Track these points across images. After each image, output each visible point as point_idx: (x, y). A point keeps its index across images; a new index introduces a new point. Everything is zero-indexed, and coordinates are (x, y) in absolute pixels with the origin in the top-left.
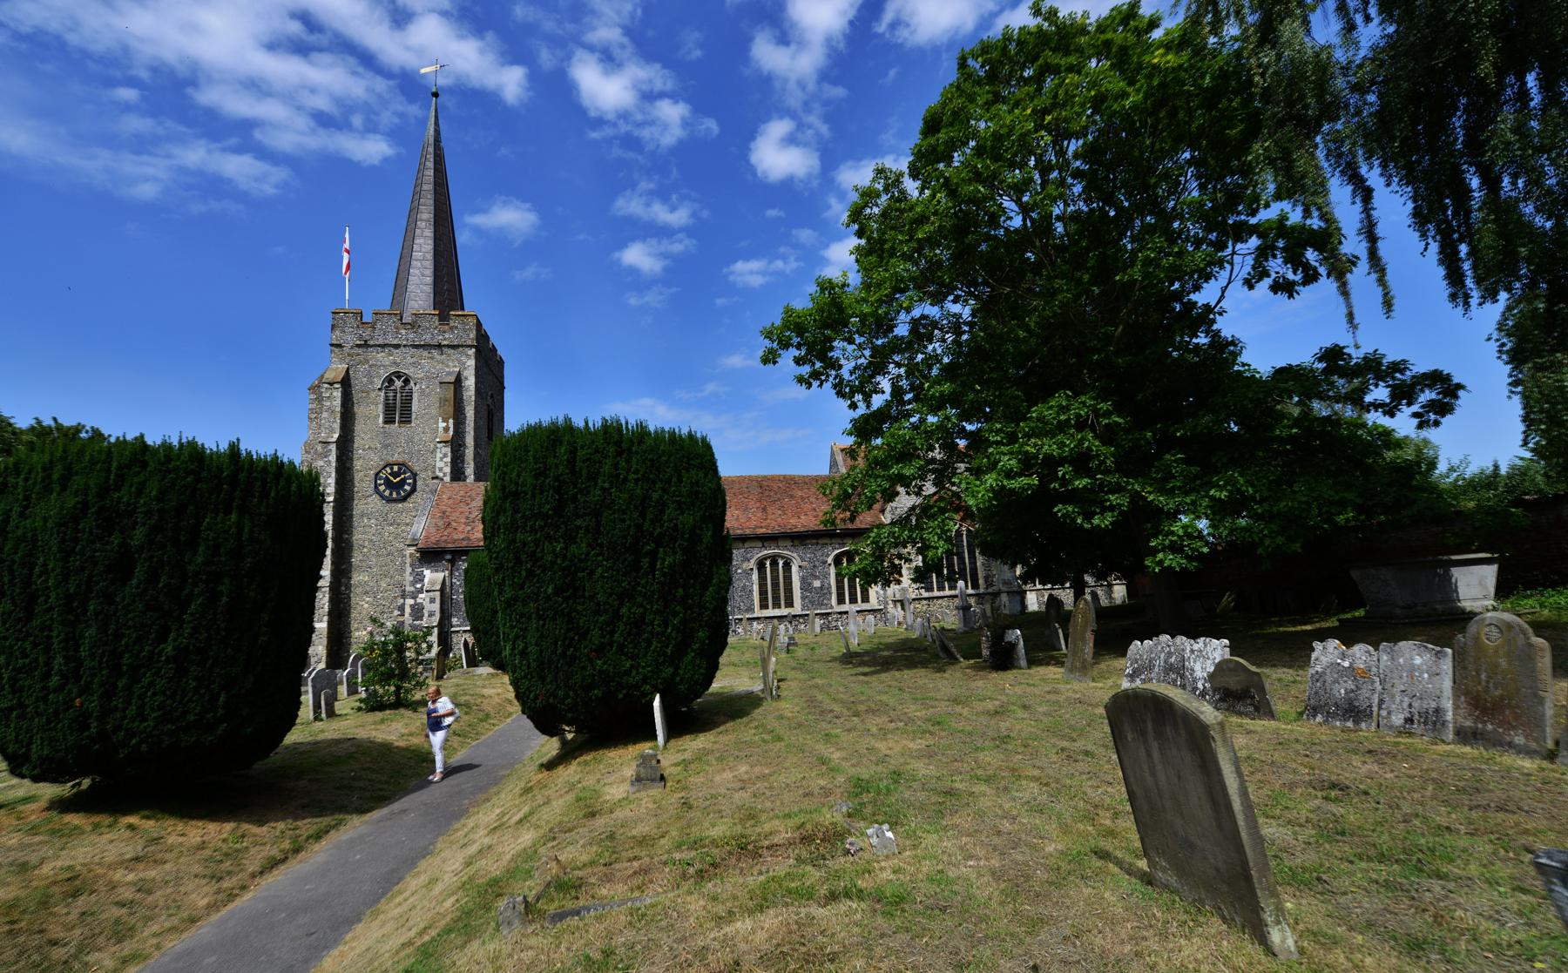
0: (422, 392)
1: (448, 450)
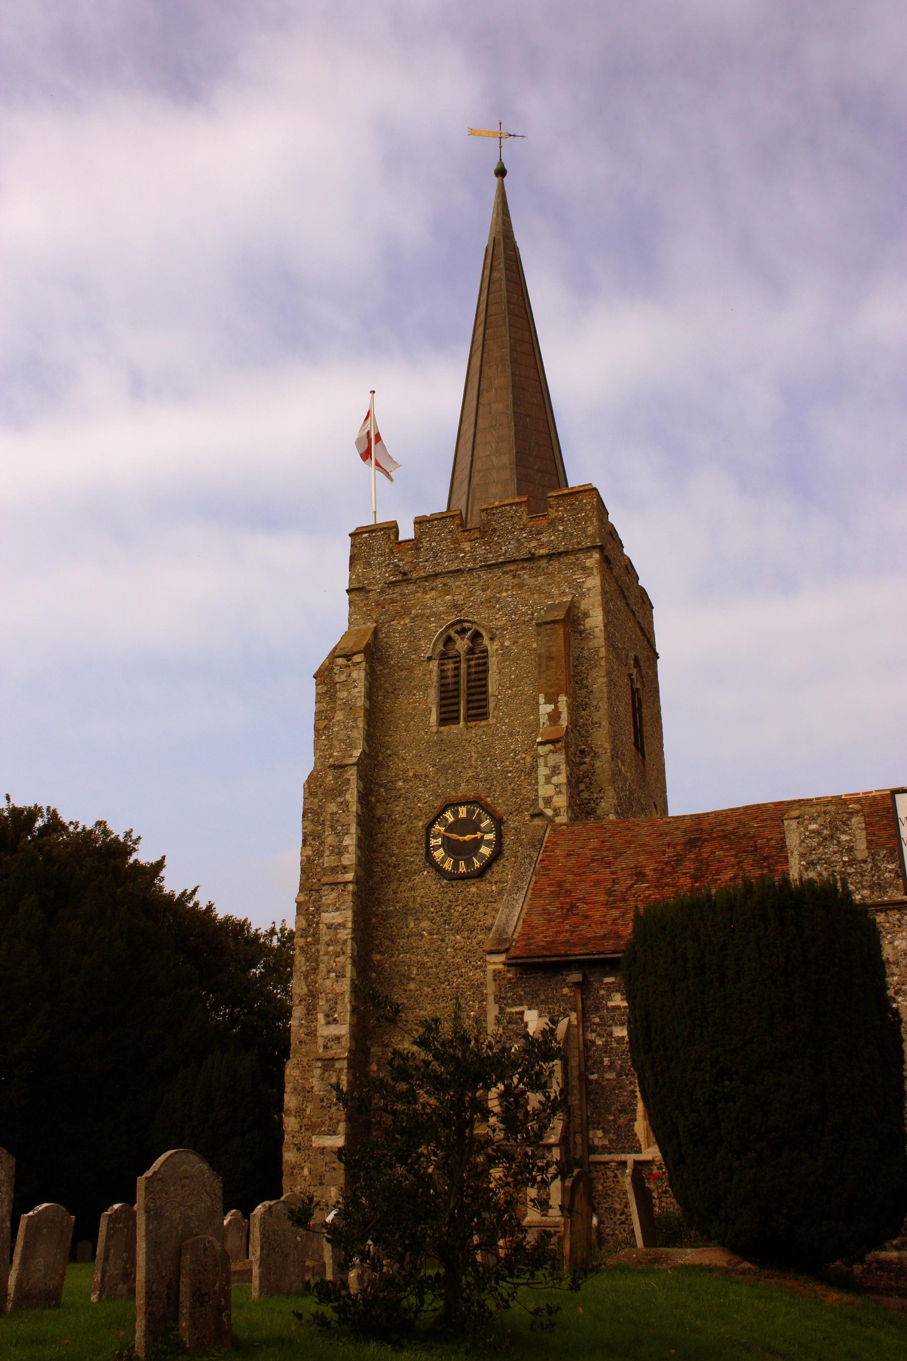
0: (505, 653)
1: (559, 758)
